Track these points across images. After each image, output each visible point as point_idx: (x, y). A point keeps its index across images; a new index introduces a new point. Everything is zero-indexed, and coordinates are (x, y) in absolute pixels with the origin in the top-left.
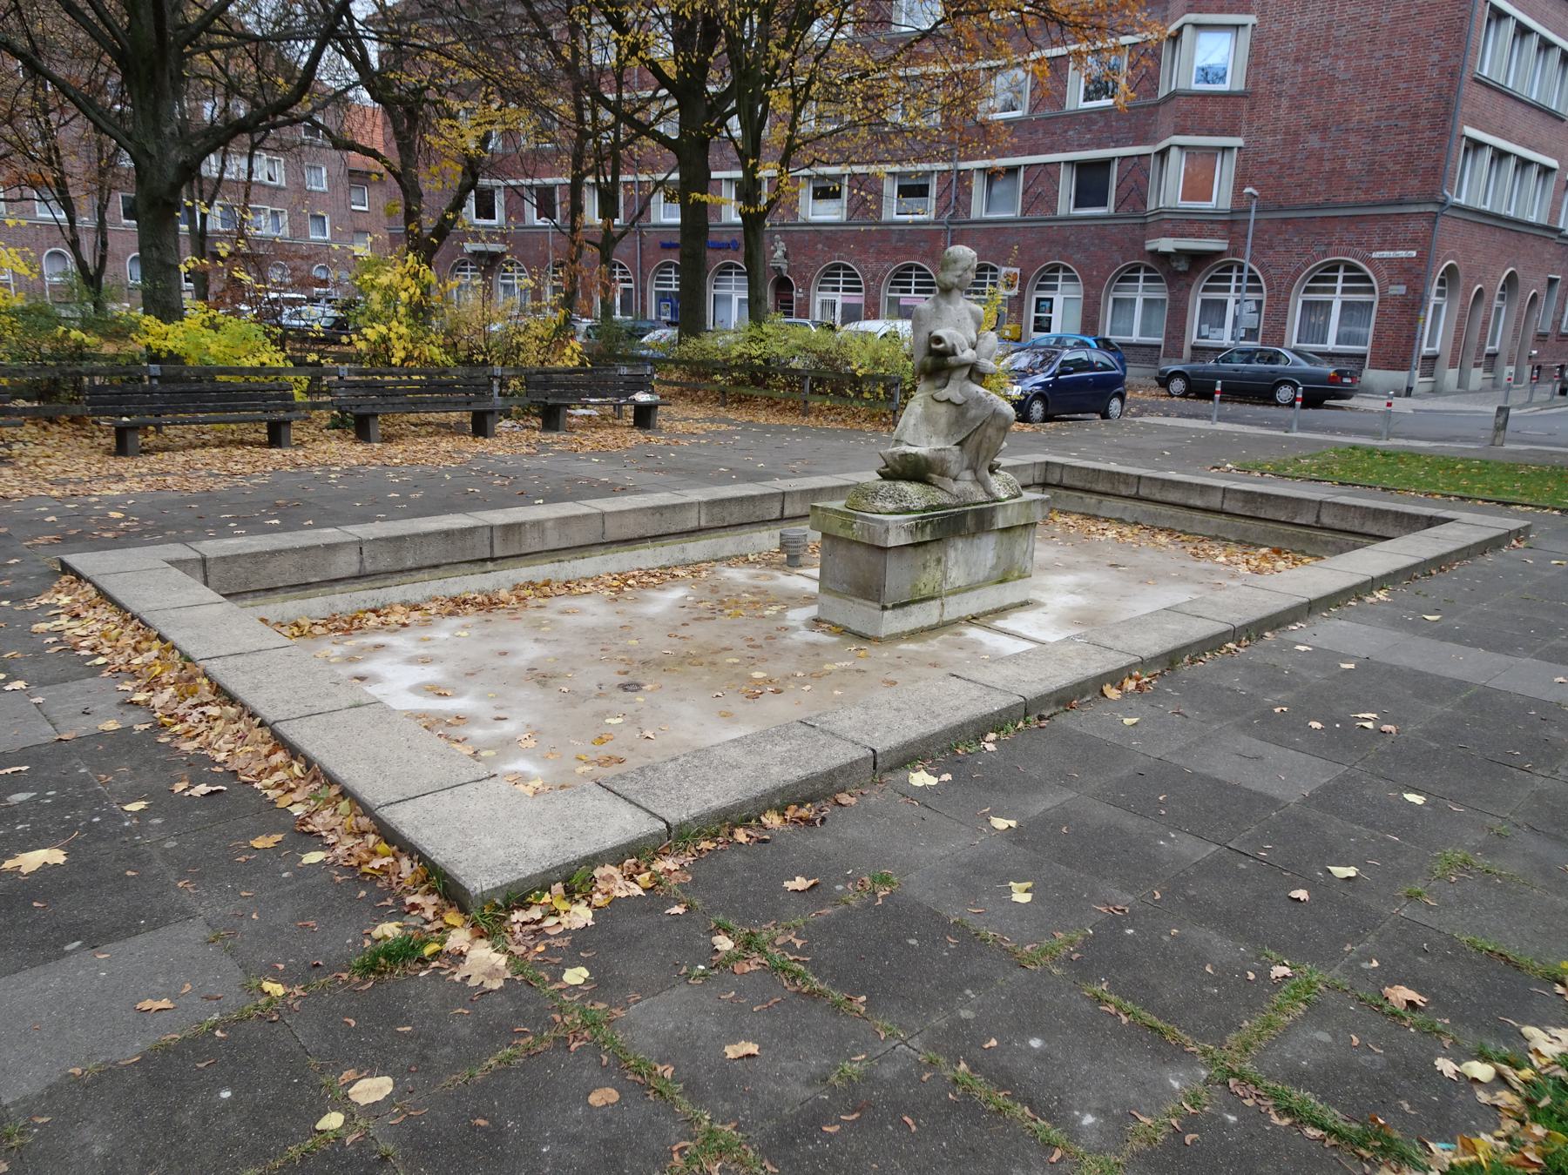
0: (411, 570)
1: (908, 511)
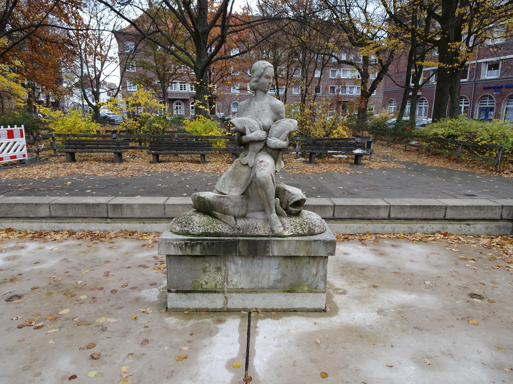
0: (70, 218)
1: (187, 233)
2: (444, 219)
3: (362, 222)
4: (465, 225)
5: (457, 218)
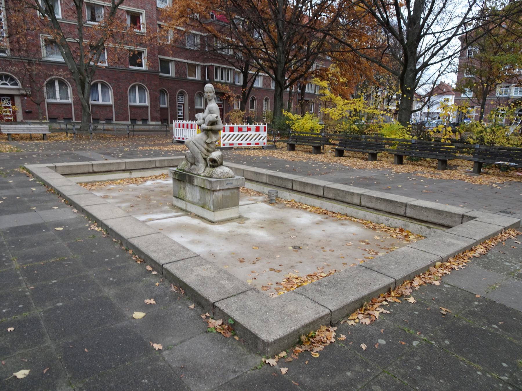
2: (404, 216)
3: (343, 204)
4: (426, 228)
5: (416, 218)
